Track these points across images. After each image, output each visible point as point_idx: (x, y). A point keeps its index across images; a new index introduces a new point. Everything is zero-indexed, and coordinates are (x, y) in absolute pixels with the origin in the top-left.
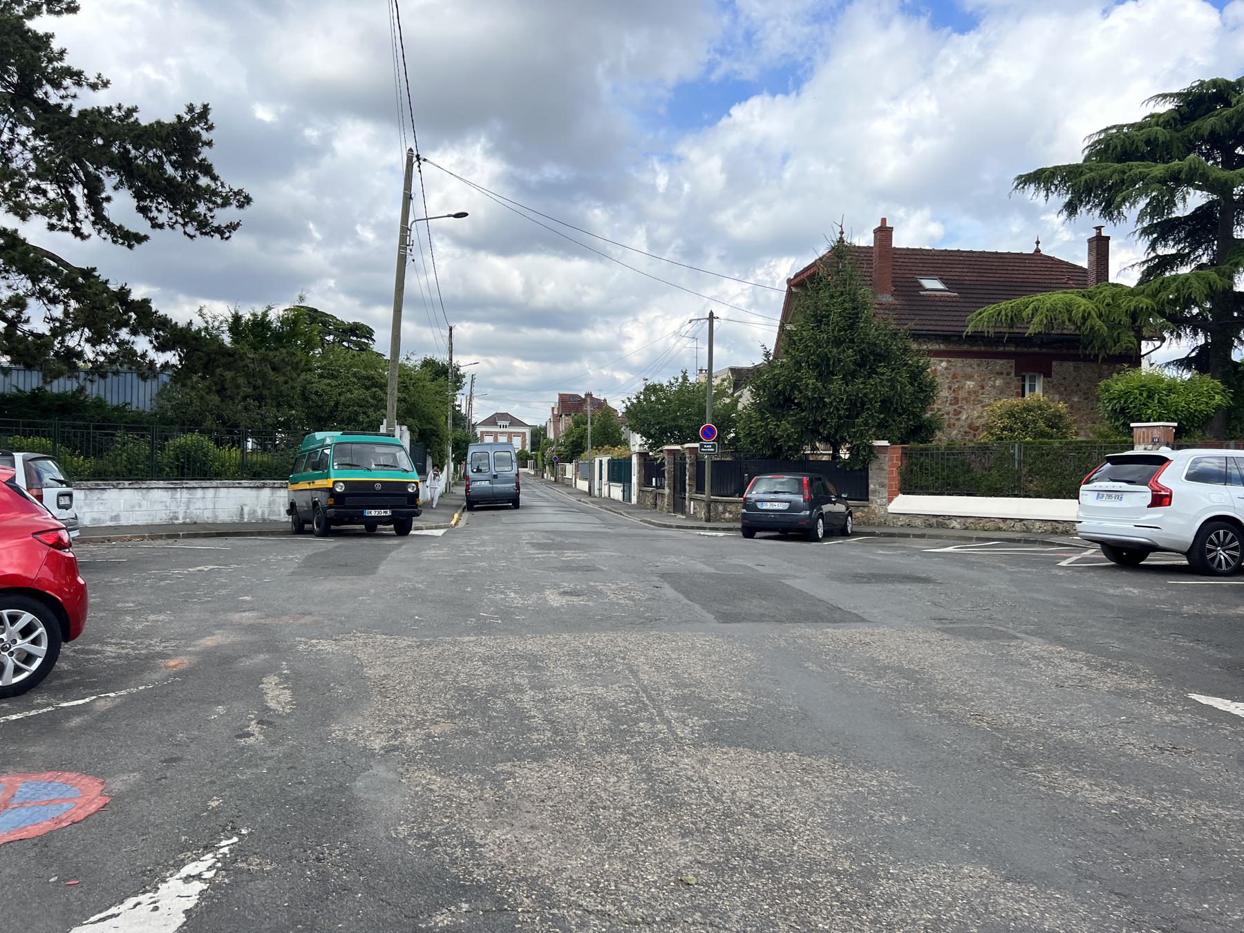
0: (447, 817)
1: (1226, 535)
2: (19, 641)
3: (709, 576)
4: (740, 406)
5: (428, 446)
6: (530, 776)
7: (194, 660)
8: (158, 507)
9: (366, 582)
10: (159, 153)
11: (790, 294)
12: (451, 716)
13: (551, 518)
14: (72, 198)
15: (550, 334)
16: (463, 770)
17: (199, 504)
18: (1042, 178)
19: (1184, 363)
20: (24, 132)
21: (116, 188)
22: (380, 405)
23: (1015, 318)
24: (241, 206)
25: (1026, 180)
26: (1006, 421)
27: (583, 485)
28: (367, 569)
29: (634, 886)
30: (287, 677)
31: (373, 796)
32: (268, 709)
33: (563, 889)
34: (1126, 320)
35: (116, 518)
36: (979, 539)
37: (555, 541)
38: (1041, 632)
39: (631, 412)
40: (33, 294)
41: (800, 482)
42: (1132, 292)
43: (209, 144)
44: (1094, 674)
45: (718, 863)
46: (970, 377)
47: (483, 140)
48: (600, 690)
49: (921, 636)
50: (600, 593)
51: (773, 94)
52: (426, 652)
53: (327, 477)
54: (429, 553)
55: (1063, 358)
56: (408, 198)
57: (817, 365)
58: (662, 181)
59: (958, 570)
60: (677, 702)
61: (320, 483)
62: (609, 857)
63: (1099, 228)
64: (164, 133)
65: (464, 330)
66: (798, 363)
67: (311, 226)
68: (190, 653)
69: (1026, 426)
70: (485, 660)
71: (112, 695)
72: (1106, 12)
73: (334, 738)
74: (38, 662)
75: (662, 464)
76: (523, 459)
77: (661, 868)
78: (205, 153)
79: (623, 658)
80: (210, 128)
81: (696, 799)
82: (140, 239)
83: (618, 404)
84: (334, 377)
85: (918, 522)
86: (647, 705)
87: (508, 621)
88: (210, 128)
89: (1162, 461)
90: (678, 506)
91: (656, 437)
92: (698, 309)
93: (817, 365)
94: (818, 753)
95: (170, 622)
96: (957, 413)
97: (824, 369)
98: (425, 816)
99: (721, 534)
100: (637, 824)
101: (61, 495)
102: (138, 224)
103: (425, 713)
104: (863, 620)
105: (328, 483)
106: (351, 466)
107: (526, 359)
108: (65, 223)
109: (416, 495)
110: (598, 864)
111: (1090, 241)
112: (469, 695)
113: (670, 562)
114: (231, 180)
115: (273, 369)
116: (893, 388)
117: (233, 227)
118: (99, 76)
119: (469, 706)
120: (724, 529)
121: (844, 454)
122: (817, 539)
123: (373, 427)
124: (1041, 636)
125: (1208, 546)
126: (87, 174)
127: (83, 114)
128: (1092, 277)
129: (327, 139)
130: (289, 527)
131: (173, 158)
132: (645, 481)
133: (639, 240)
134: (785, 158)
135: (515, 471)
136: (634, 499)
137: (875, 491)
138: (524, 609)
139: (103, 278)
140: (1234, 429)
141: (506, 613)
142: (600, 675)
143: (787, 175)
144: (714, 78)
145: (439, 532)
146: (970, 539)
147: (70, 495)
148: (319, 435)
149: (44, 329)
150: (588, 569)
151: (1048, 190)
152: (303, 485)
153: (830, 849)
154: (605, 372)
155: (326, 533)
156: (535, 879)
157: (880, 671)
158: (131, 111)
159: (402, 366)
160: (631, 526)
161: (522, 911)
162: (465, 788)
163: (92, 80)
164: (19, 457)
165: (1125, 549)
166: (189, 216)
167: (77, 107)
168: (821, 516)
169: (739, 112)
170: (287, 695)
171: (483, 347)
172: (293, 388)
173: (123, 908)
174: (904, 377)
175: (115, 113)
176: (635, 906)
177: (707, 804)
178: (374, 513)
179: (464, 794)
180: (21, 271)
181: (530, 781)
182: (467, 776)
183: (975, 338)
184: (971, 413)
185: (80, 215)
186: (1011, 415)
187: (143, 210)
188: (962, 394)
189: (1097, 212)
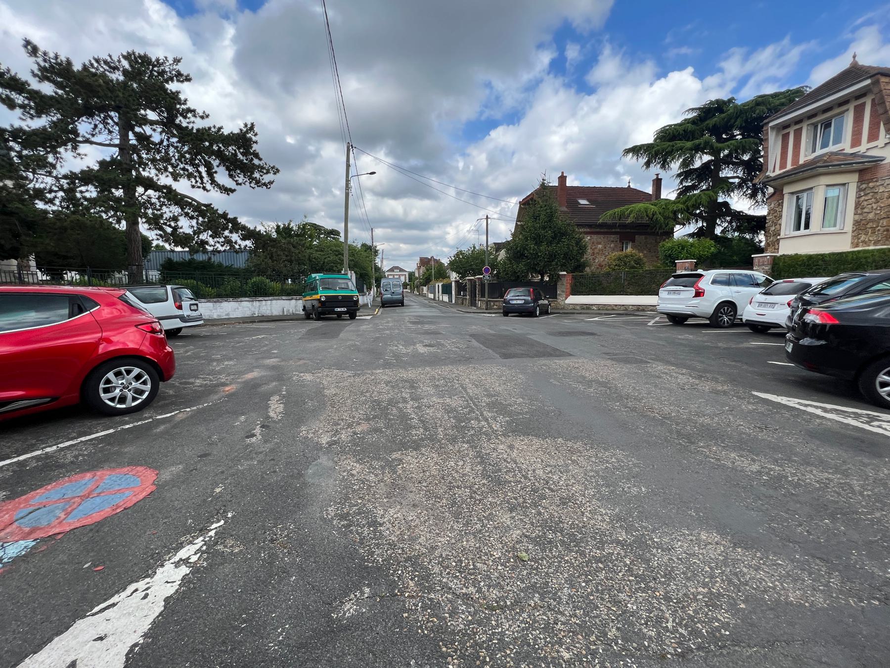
0: (360, 498)
1: (728, 309)
2: (133, 383)
3: (494, 335)
4: (499, 259)
5: (364, 280)
6: (411, 461)
7: (239, 386)
8: (245, 309)
9: (334, 343)
10: (234, 148)
11: (520, 207)
12: (368, 419)
13: (416, 310)
14: (200, 173)
15: (415, 233)
16: (373, 458)
17: (265, 308)
18: (636, 150)
19: (692, 235)
20: (175, 140)
21: (218, 166)
22: (342, 263)
23: (622, 216)
24: (275, 174)
25: (628, 151)
26: (617, 262)
27: (431, 296)
28: (334, 335)
29: (485, 564)
30: (284, 396)
31: (316, 481)
32: (269, 417)
33: (437, 569)
34: (671, 215)
35: (228, 314)
36: (606, 314)
37: (420, 321)
38: (658, 359)
39: (452, 263)
40: (182, 215)
41: (529, 291)
42: (674, 202)
43: (256, 142)
44: (697, 382)
45: (539, 537)
46: (600, 243)
47: (384, 149)
48: (448, 400)
49: (602, 362)
50: (443, 345)
51: (508, 125)
52: (357, 380)
53: (317, 294)
54: (364, 327)
55: (640, 234)
56: (348, 166)
57: (535, 239)
58: (461, 165)
59: (605, 329)
60: (491, 406)
61: (315, 297)
62: (465, 533)
63: (657, 175)
64: (235, 138)
65: (378, 232)
66: (526, 238)
67: (313, 189)
68: (238, 383)
69: (626, 264)
70: (387, 383)
71: (188, 410)
72: (651, 84)
73: (301, 436)
74: (146, 394)
75: (466, 285)
76: (405, 285)
77: (501, 543)
78: (255, 147)
79: (458, 380)
80: (256, 135)
81: (513, 477)
82: (233, 191)
83: (445, 261)
84: (322, 251)
85: (578, 307)
86: (473, 409)
87: (399, 362)
88: (256, 135)
89: (700, 276)
90: (473, 303)
91: (463, 275)
92: (482, 214)
93: (535, 239)
94: (575, 438)
95: (235, 365)
96: (594, 259)
97: (538, 240)
98: (347, 498)
99: (493, 315)
100: (480, 500)
101: (191, 305)
102: (228, 183)
103: (354, 417)
104: (571, 355)
105: (318, 297)
106: (329, 289)
107: (405, 243)
108: (199, 184)
109: (358, 301)
110: (459, 540)
111: (653, 181)
112: (378, 405)
113: (474, 328)
114: (267, 160)
115: (294, 247)
116: (568, 248)
117: (271, 183)
118: (204, 112)
119: (378, 412)
120: (494, 313)
121: (546, 279)
122: (537, 316)
123: (339, 272)
124: (660, 361)
125: (720, 315)
126: (205, 161)
127: (198, 130)
128: (654, 197)
129: (318, 150)
130: (304, 316)
131: (241, 150)
132: (458, 293)
133: (452, 192)
134: (513, 153)
135: (402, 290)
136: (454, 301)
137: (560, 294)
138: (407, 354)
139: (215, 208)
140: (714, 263)
141: (397, 356)
142: (447, 391)
143: (514, 161)
144: (483, 118)
145: (369, 317)
146: (601, 314)
147: (197, 305)
148: (313, 275)
149: (190, 231)
150: (435, 333)
151: (638, 156)
152: (308, 298)
153: (607, 518)
154: (439, 248)
155: (319, 319)
156: (417, 557)
157: (589, 383)
158: (220, 129)
159: (349, 246)
160: (453, 313)
161: (409, 596)
162: (373, 473)
163: (201, 114)
164: (169, 287)
165: (676, 317)
166: (252, 179)
167: (196, 127)
168: (538, 306)
169: (494, 134)
170: (281, 408)
171: (389, 239)
172: (305, 256)
173: (123, 595)
174: (573, 242)
175: (213, 129)
176: (489, 587)
177: (520, 481)
178: (339, 309)
179: (372, 477)
180: (176, 204)
181: (412, 466)
182: (375, 464)
183: (602, 226)
184: (600, 259)
185: (205, 180)
186: (619, 259)
187: (231, 176)
188: (596, 251)
189: (659, 166)
